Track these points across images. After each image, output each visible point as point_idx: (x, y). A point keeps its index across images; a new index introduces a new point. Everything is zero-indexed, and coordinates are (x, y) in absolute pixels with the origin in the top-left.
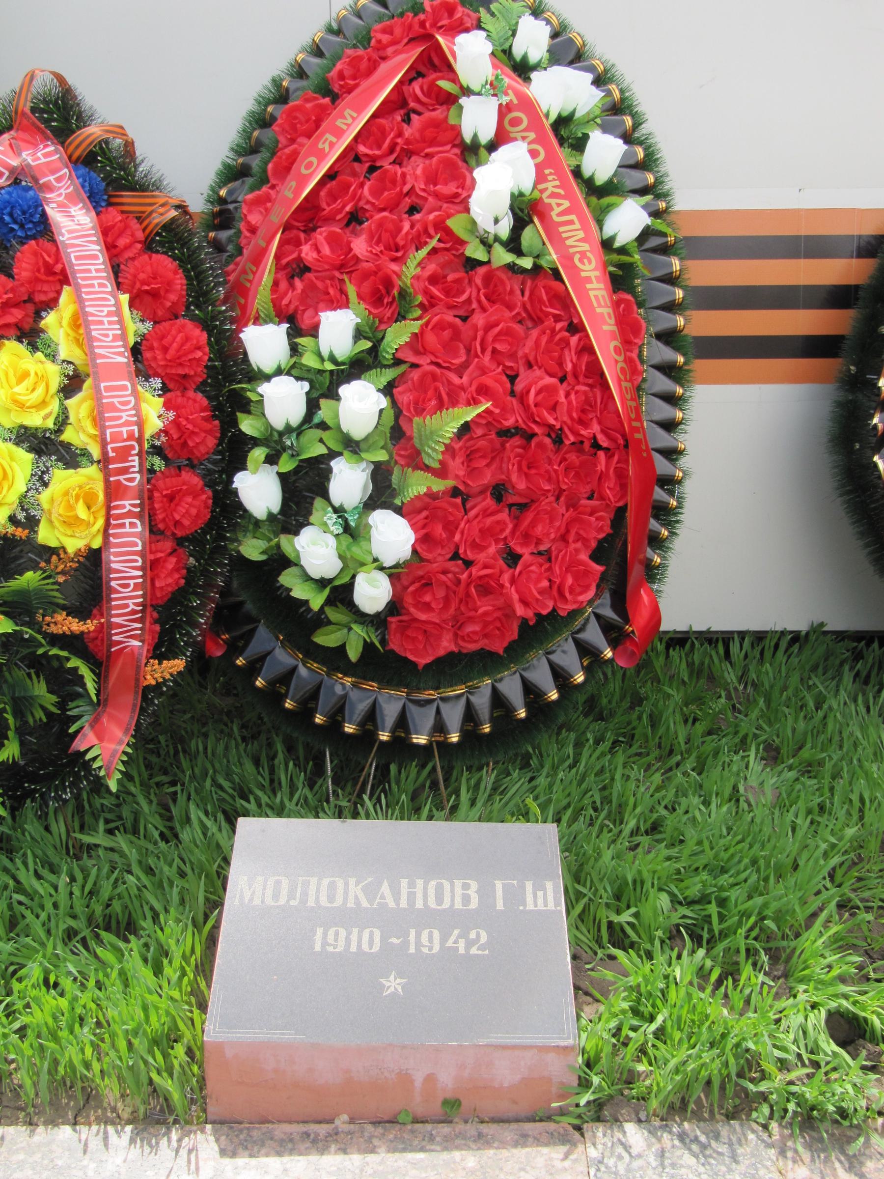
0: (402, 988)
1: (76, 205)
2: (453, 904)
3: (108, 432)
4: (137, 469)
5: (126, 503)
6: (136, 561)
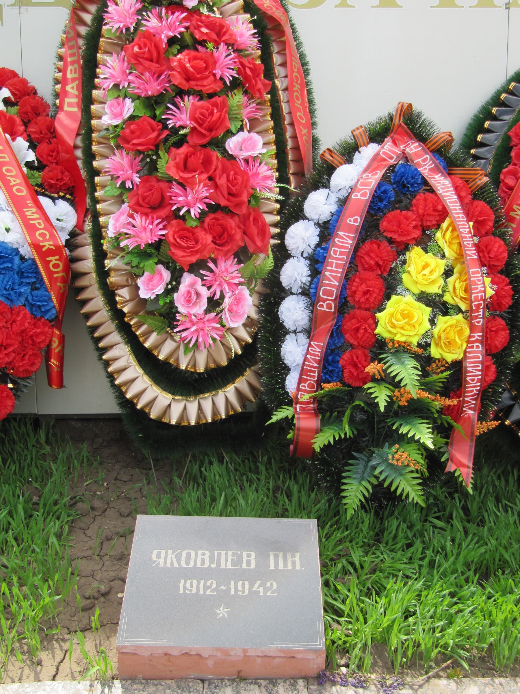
0: (216, 612)
1: (437, 174)
2: (195, 564)
3: (473, 296)
4: (481, 316)
5: (476, 335)
6: (479, 366)
